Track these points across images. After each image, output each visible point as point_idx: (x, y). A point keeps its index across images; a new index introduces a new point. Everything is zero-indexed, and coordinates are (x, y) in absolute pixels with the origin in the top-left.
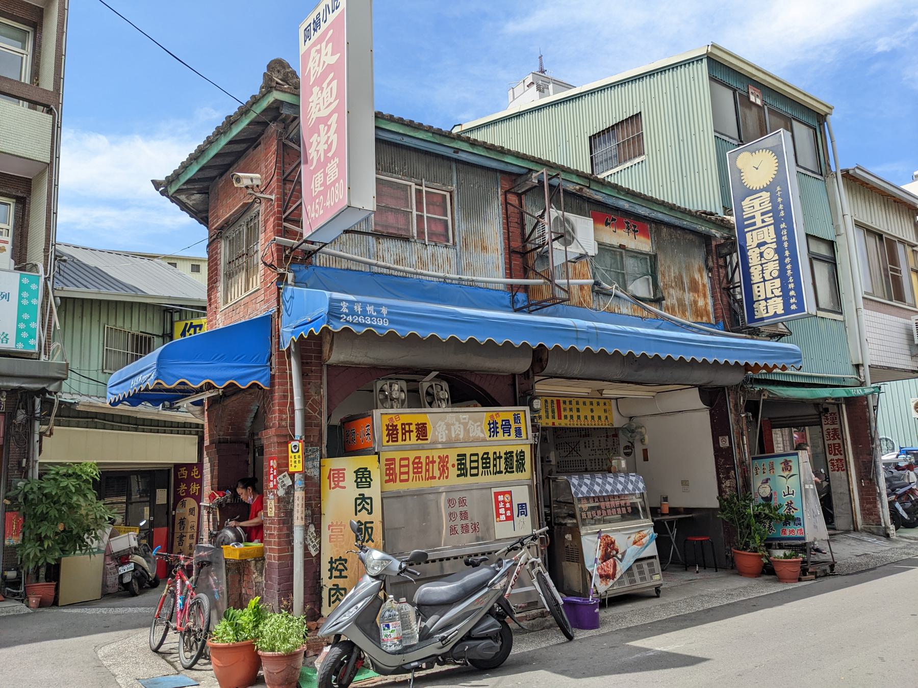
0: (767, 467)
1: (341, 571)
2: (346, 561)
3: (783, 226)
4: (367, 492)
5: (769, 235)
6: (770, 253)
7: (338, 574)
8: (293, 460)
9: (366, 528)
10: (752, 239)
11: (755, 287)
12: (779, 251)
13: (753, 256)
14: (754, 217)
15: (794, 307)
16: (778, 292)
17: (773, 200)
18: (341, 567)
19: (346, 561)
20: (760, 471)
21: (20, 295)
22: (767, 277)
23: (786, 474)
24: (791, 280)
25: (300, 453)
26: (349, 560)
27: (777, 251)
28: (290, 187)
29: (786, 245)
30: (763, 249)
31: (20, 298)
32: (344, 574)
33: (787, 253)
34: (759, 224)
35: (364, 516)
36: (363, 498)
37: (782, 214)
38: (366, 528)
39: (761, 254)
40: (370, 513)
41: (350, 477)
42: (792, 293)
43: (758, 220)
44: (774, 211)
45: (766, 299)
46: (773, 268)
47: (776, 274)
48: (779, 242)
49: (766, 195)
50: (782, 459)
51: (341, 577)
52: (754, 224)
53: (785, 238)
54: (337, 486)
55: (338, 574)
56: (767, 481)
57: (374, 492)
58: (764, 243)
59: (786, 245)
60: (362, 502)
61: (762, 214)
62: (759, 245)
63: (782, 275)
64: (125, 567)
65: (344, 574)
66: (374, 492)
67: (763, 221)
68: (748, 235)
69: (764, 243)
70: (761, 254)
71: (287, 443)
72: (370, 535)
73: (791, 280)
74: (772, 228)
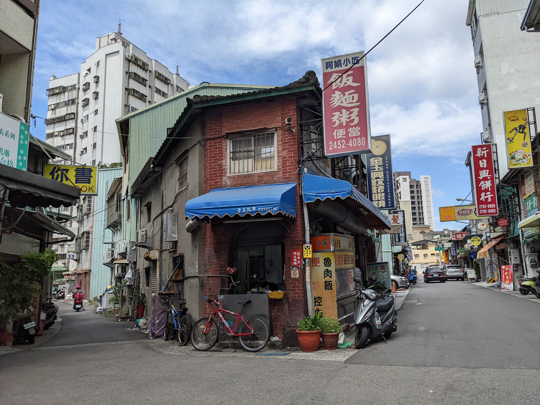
0: (374, 268)
1: (319, 302)
2: (321, 298)
3: (387, 172)
4: (329, 268)
5: (381, 175)
6: (381, 182)
7: (318, 304)
8: (306, 252)
9: (329, 284)
10: (373, 175)
11: (373, 195)
12: (385, 182)
13: (374, 182)
14: (375, 166)
15: (390, 205)
16: (383, 198)
17: (384, 161)
18: (319, 301)
19: (321, 298)
20: (371, 270)
21: (20, 137)
22: (379, 191)
23: (382, 271)
24: (389, 194)
25: (311, 249)
26: (323, 298)
27: (384, 182)
28: (140, 97)
29: (388, 180)
30: (378, 180)
31: (20, 139)
32: (321, 304)
33: (388, 183)
34: (377, 170)
35: (328, 279)
36: (327, 271)
37: (387, 168)
38: (329, 284)
39: (377, 182)
40: (331, 277)
41: (322, 262)
42: (389, 199)
43: (377, 168)
44: (384, 166)
45: (378, 200)
46: (381, 188)
47: (383, 191)
48: (385, 178)
49: (381, 159)
50: (381, 265)
51: (319, 305)
52: (375, 169)
53: (388, 177)
54: (316, 265)
55: (318, 304)
56: (374, 273)
57: (332, 268)
58: (379, 178)
59: (388, 180)
60: (327, 273)
61: (379, 166)
62: (376, 178)
63: (385, 192)
64: (29, 324)
65: (321, 304)
66: (332, 268)
67: (379, 169)
68: (372, 173)
69: (379, 178)
70: (377, 182)
71: (303, 245)
72: (331, 287)
73: (389, 194)
74: (382, 172)
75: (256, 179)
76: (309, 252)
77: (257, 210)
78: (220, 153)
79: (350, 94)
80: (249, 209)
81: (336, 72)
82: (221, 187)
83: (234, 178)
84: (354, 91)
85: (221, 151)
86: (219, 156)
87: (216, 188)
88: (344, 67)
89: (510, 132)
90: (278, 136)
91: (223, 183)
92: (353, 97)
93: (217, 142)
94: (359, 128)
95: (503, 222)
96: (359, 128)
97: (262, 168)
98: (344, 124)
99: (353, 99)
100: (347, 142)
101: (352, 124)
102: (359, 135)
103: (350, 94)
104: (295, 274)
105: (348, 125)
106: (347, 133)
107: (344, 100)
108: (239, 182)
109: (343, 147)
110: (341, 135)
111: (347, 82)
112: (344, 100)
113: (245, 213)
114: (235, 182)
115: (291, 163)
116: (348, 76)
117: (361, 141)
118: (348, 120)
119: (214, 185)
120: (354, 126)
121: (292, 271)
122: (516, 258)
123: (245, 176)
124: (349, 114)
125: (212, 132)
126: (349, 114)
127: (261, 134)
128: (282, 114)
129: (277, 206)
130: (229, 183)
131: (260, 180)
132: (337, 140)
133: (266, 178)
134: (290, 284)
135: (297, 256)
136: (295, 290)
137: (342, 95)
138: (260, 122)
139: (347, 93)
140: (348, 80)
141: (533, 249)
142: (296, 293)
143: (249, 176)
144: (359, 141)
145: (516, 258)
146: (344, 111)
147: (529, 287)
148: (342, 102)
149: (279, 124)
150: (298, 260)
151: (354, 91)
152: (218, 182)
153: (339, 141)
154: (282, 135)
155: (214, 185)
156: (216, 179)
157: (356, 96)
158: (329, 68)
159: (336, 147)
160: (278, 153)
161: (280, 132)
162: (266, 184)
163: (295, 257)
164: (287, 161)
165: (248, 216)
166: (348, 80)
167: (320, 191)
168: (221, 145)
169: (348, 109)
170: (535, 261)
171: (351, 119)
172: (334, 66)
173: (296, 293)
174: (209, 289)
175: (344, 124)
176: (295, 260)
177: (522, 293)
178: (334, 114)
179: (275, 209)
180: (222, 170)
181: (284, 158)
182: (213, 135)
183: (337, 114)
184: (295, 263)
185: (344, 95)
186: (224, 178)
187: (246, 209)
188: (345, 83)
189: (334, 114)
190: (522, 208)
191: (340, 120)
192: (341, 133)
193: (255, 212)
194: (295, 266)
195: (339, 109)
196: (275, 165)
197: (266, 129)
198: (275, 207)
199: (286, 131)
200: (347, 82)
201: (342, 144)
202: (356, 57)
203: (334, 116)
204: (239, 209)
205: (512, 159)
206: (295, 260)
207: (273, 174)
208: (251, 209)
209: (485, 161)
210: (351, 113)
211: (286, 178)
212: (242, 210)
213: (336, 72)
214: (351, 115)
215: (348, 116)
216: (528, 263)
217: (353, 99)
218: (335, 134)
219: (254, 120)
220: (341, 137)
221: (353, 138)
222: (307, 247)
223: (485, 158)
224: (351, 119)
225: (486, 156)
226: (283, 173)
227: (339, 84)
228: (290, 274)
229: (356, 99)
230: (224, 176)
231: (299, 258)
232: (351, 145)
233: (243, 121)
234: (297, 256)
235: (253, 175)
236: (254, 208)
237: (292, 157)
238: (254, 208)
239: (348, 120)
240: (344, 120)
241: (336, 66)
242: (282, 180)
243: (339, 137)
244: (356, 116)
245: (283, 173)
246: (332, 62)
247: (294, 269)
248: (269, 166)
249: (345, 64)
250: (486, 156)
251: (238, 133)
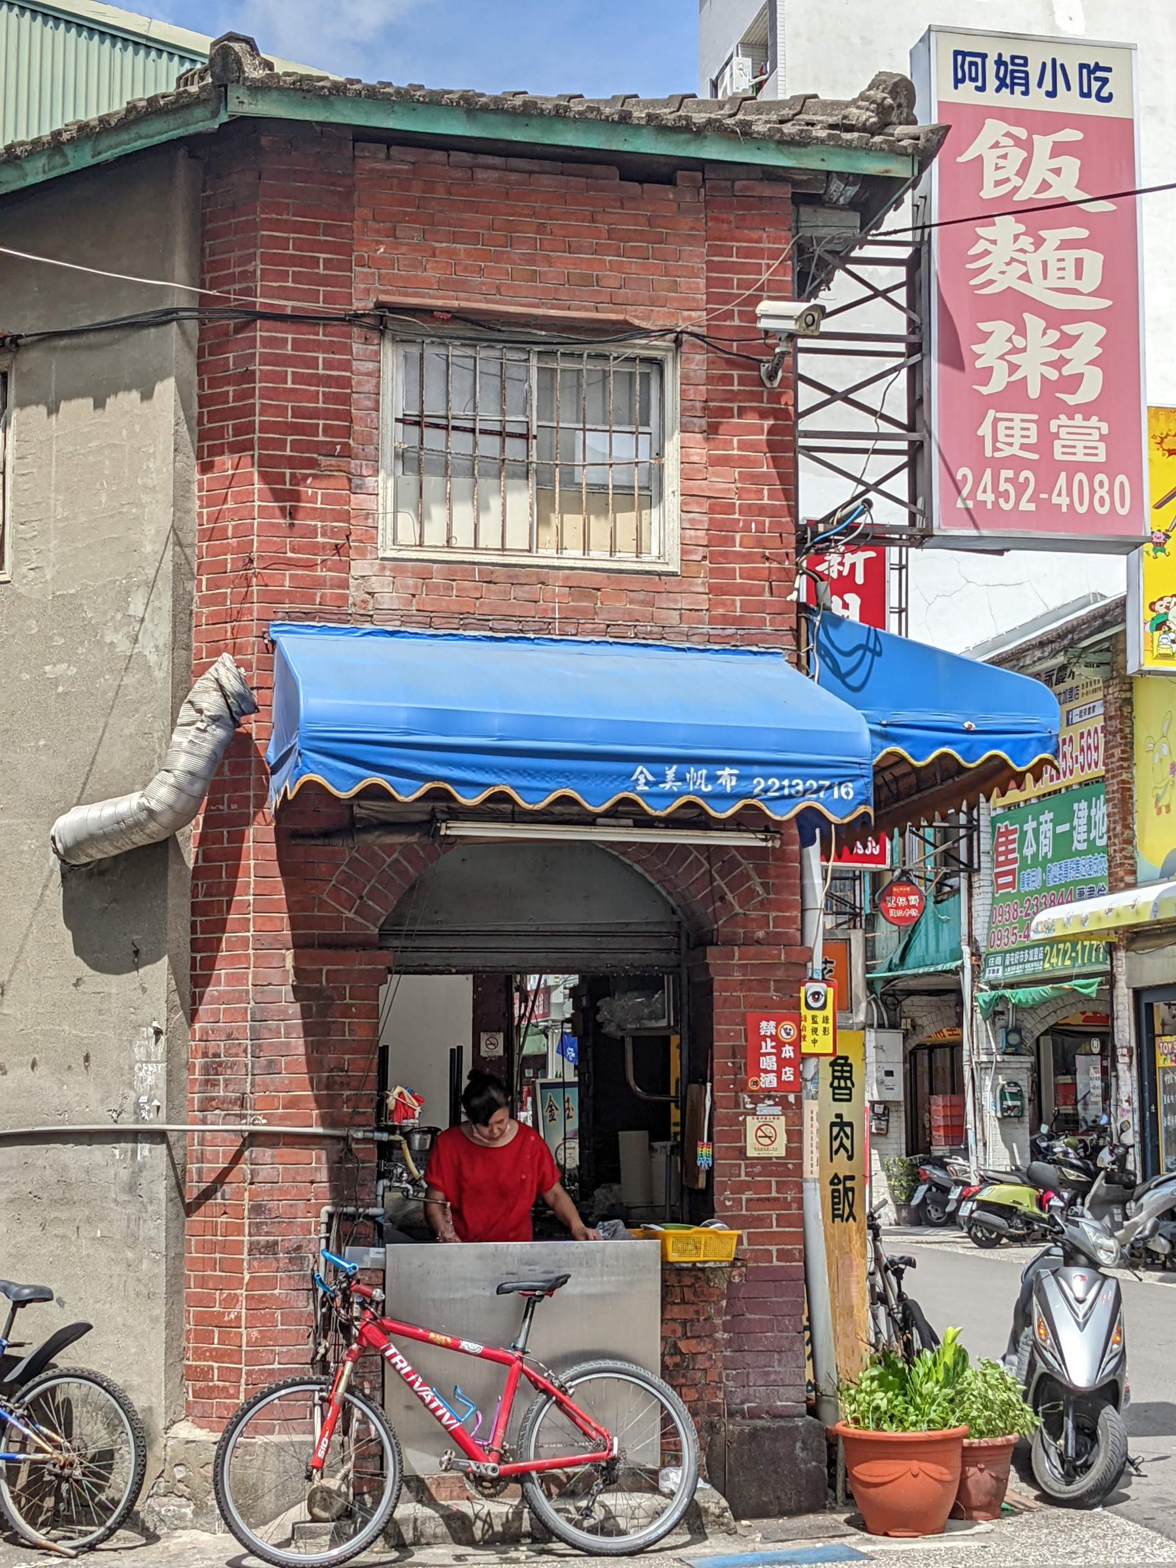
25: (829, 1011)
36: (840, 1123)
75: (556, 599)
76: (820, 1026)
77: (744, 787)
78: (337, 415)
79: (1065, 245)
80: (697, 777)
81: (1001, 114)
82: (343, 617)
83: (423, 571)
84: (1083, 233)
85: (346, 400)
86: (327, 430)
87: (307, 615)
88: (1037, 101)
89: (1159, 506)
90: (686, 381)
91: (355, 593)
92: (1079, 262)
93: (318, 346)
94: (1105, 428)
95: (902, 901)
96: (1105, 431)
97: (580, 544)
98: (1034, 391)
99: (1079, 276)
100: (1046, 483)
101: (1071, 400)
102: (1102, 458)
103: (1065, 245)
104: (764, 1135)
105: (1051, 402)
106: (1047, 438)
107: (1036, 272)
108: (452, 602)
109: (1026, 506)
110: (1017, 441)
111: (1051, 178)
112: (1036, 272)
113: (674, 795)
114: (427, 600)
115: (760, 543)
116: (1059, 150)
117: (1111, 492)
118: (1053, 375)
119: (290, 596)
120: (1079, 408)
121: (752, 1123)
122: (889, 1073)
123: (489, 576)
124: (1056, 346)
125: (283, 276)
126: (1056, 346)
127: (587, 349)
128: (712, 266)
129: (853, 778)
130: (388, 597)
131: (583, 611)
132: (998, 465)
133: (617, 606)
134: (741, 1187)
135: (779, 1045)
136: (762, 1221)
137: (1026, 242)
138: (586, 281)
139: (1052, 236)
140: (1057, 171)
141: (1014, 1039)
142: (772, 1238)
143: (515, 574)
144: (1102, 492)
145: (889, 1073)
146: (1034, 323)
147: (1006, 1211)
148: (1025, 277)
149: (695, 319)
150: (782, 1063)
151: (1083, 233)
152: (319, 583)
153: (1006, 473)
154: (710, 380)
155: (290, 596)
156: (311, 566)
157: (1094, 261)
158: (969, 85)
159: (989, 498)
160: (685, 477)
161: (698, 362)
162: (614, 635)
163: (768, 1046)
164: (732, 527)
165: (692, 817)
166: (1057, 171)
167: (906, 717)
168: (347, 365)
169: (1055, 318)
170: (1017, 1096)
171: (1067, 371)
172: (992, 83)
173: (772, 1238)
174: (257, 1209)
175: (1034, 391)
176: (768, 1063)
177: (975, 1239)
178: (984, 326)
179: (847, 791)
180: (346, 517)
181: (717, 505)
182: (286, 294)
183: (1001, 330)
184: (769, 1081)
185: (1039, 242)
186: (359, 568)
187: (680, 778)
188: (1045, 186)
189: (984, 326)
190: (986, 842)
191: (1014, 368)
192: (1014, 433)
193: (735, 796)
194: (768, 1094)
195: (1013, 306)
196: (662, 535)
197: (624, 330)
198: (842, 780)
199: (731, 364)
200: (1051, 178)
201: (1021, 489)
202: (1098, 67)
203: (985, 337)
204: (642, 773)
205: (1159, 627)
206: (768, 1063)
207: (655, 581)
208: (712, 778)
209: (853, 600)
210: (1067, 341)
211: (725, 620)
212: (661, 778)
213: (1001, 114)
214: (1066, 353)
215: (1054, 355)
216: (988, 1099)
217: (1079, 276)
218: (985, 430)
219: (549, 262)
220: (1015, 450)
221: (1072, 468)
222: (816, 996)
223: (856, 589)
224: (1067, 371)
225: (860, 579)
226: (713, 589)
227: (1017, 181)
228: (741, 1135)
229: (1093, 276)
230: (362, 554)
231: (788, 1052)
232: (1064, 501)
233: (487, 256)
234: (779, 1045)
235: (541, 575)
236: (728, 778)
237: (762, 510)
238: (728, 778)
239: (1053, 375)
240: (1034, 370)
241: (1002, 84)
242: (706, 628)
243: (1008, 451)
244: (1091, 363)
245: (713, 589)
246: (984, 56)
247: (762, 1108)
248: (626, 539)
249: (1048, 85)
250: (860, 579)
251: (458, 316)
